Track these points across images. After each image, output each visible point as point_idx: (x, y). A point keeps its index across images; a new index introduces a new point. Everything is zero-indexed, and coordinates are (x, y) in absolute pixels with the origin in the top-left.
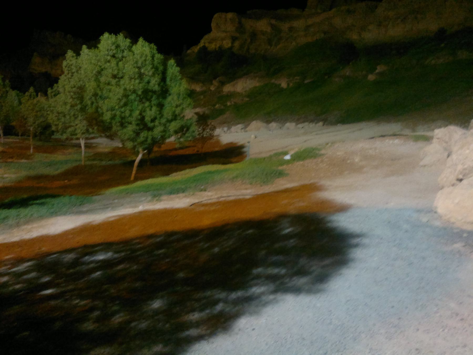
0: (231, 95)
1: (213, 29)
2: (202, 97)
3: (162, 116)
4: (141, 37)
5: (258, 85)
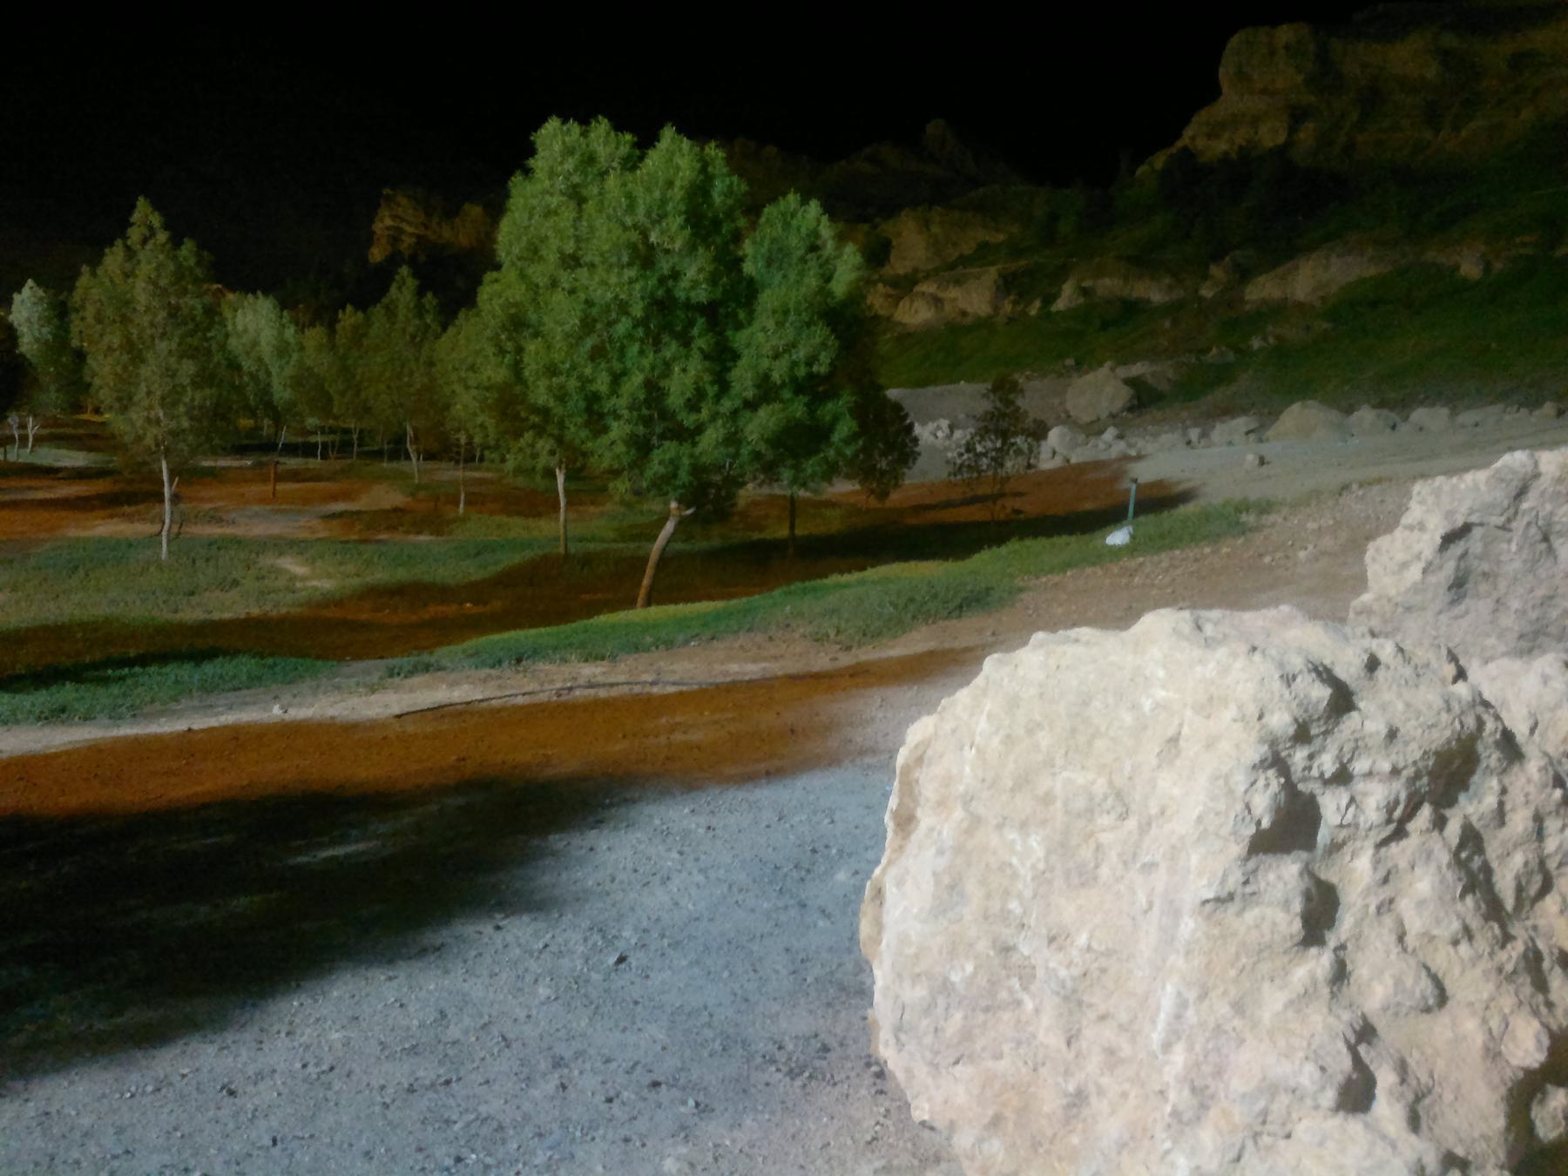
0: (1276, 311)
1: (1225, 88)
2: (1167, 324)
3: (724, 387)
4: (670, 124)
5: (1372, 271)
